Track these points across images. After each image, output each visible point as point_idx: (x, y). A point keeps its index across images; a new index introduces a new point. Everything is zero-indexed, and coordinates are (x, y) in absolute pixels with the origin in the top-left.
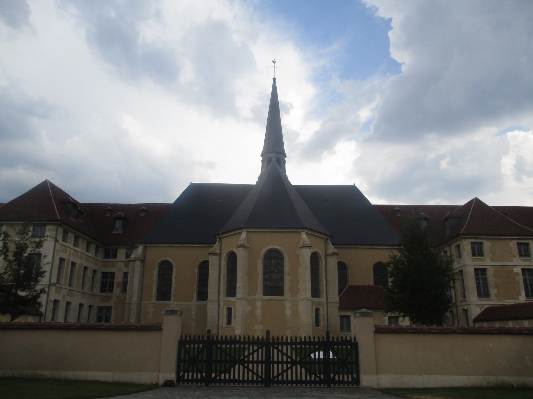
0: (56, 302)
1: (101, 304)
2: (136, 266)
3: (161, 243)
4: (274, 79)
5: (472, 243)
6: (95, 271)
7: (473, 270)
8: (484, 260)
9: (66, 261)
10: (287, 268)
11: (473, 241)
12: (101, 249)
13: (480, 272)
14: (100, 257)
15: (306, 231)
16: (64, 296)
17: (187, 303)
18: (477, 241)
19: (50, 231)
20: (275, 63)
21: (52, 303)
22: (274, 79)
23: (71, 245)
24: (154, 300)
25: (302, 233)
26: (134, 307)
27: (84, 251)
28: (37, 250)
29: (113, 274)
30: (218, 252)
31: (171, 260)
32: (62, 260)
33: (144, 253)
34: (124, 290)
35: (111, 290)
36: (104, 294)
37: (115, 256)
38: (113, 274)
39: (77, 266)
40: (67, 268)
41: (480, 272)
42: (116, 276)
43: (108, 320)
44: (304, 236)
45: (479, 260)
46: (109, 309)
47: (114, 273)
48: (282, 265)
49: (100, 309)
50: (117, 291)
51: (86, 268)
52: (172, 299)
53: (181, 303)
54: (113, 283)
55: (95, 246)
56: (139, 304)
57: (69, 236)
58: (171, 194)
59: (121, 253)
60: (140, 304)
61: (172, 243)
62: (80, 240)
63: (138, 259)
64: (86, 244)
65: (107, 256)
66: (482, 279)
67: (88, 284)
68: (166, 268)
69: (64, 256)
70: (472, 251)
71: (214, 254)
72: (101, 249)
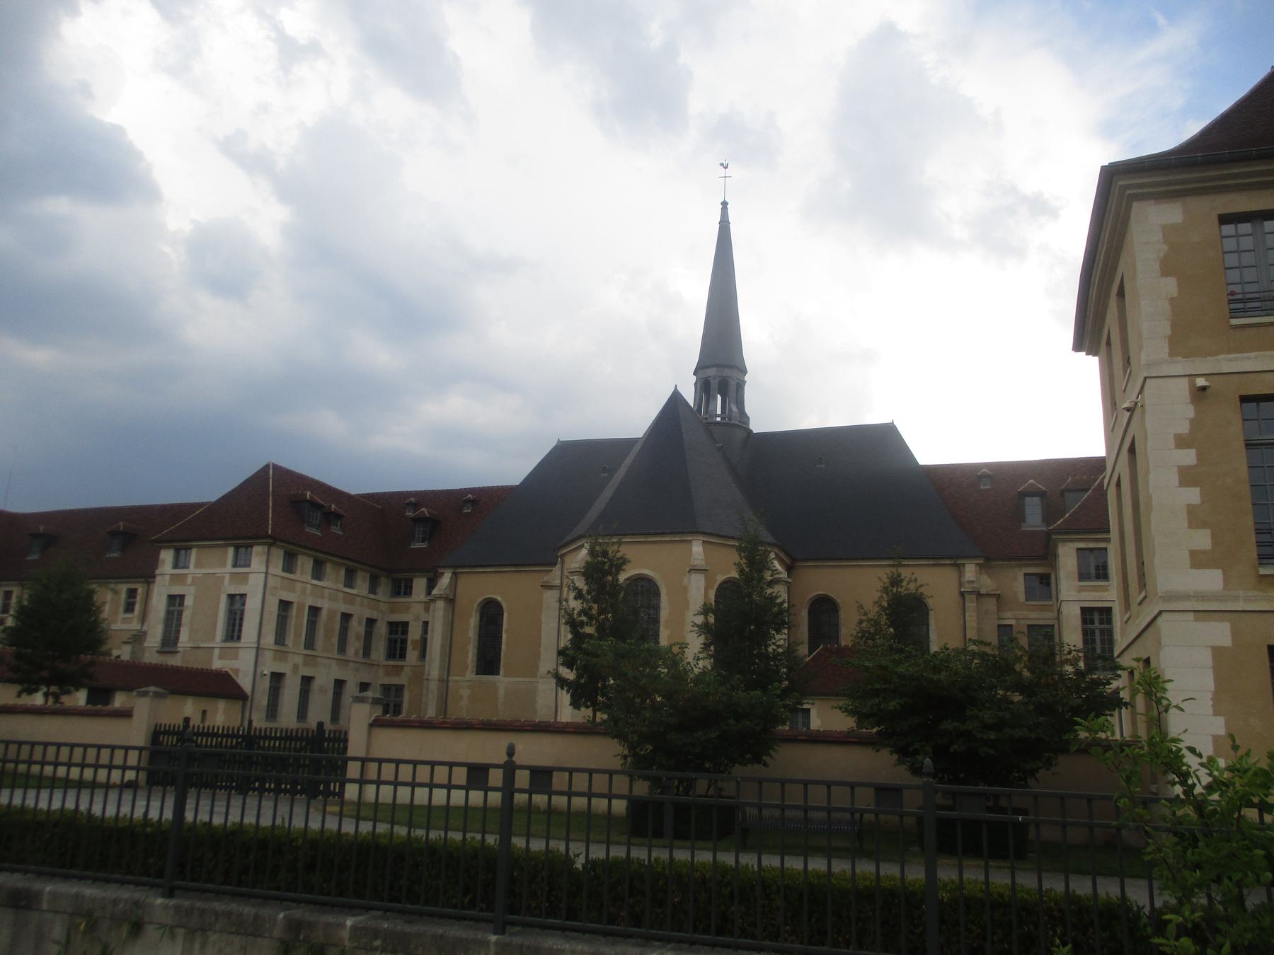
0: (277, 678)
1: (387, 681)
2: (438, 612)
3: (482, 566)
4: (725, 204)
5: (1078, 549)
6: (371, 622)
7: (1078, 612)
8: (1105, 589)
9: (295, 606)
10: (664, 614)
11: (1082, 545)
12: (383, 580)
13: (1096, 617)
14: (383, 594)
15: (702, 538)
16: (296, 667)
17: (528, 680)
18: (1091, 545)
19: (258, 556)
20: (726, 168)
21: (268, 679)
22: (725, 204)
23: (307, 577)
24: (470, 675)
25: (694, 543)
26: (433, 686)
27: (341, 586)
28: (580, 557)
29: (405, 625)
30: (557, 582)
31: (499, 599)
32: (285, 605)
33: (454, 584)
34: (423, 655)
35: (403, 656)
36: (391, 663)
37: (408, 591)
38: (405, 625)
39: (324, 613)
40: (299, 621)
41: (1096, 617)
42: (410, 629)
43: (397, 709)
44: (697, 548)
45: (1095, 589)
46: (400, 689)
47: (406, 624)
48: (657, 608)
49: (386, 688)
50: (412, 655)
51: (346, 617)
52: (502, 672)
53: (516, 679)
54: (404, 642)
55: (368, 576)
56: (444, 682)
57: (299, 562)
58: (513, 470)
59: (420, 584)
60: (448, 681)
61: (500, 566)
62: (329, 568)
63: (440, 597)
64: (343, 572)
65: (397, 593)
66: (1102, 632)
67: (354, 646)
68: (491, 614)
69: (287, 596)
70: (229, 619)
71: (551, 587)
72: (383, 580)
